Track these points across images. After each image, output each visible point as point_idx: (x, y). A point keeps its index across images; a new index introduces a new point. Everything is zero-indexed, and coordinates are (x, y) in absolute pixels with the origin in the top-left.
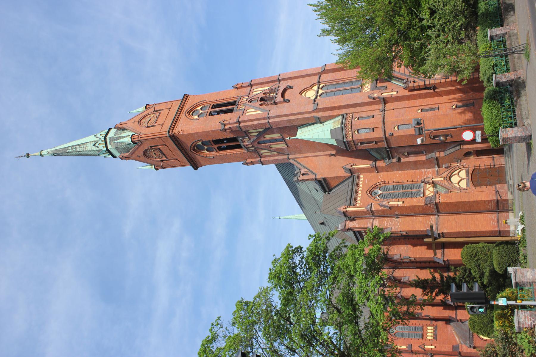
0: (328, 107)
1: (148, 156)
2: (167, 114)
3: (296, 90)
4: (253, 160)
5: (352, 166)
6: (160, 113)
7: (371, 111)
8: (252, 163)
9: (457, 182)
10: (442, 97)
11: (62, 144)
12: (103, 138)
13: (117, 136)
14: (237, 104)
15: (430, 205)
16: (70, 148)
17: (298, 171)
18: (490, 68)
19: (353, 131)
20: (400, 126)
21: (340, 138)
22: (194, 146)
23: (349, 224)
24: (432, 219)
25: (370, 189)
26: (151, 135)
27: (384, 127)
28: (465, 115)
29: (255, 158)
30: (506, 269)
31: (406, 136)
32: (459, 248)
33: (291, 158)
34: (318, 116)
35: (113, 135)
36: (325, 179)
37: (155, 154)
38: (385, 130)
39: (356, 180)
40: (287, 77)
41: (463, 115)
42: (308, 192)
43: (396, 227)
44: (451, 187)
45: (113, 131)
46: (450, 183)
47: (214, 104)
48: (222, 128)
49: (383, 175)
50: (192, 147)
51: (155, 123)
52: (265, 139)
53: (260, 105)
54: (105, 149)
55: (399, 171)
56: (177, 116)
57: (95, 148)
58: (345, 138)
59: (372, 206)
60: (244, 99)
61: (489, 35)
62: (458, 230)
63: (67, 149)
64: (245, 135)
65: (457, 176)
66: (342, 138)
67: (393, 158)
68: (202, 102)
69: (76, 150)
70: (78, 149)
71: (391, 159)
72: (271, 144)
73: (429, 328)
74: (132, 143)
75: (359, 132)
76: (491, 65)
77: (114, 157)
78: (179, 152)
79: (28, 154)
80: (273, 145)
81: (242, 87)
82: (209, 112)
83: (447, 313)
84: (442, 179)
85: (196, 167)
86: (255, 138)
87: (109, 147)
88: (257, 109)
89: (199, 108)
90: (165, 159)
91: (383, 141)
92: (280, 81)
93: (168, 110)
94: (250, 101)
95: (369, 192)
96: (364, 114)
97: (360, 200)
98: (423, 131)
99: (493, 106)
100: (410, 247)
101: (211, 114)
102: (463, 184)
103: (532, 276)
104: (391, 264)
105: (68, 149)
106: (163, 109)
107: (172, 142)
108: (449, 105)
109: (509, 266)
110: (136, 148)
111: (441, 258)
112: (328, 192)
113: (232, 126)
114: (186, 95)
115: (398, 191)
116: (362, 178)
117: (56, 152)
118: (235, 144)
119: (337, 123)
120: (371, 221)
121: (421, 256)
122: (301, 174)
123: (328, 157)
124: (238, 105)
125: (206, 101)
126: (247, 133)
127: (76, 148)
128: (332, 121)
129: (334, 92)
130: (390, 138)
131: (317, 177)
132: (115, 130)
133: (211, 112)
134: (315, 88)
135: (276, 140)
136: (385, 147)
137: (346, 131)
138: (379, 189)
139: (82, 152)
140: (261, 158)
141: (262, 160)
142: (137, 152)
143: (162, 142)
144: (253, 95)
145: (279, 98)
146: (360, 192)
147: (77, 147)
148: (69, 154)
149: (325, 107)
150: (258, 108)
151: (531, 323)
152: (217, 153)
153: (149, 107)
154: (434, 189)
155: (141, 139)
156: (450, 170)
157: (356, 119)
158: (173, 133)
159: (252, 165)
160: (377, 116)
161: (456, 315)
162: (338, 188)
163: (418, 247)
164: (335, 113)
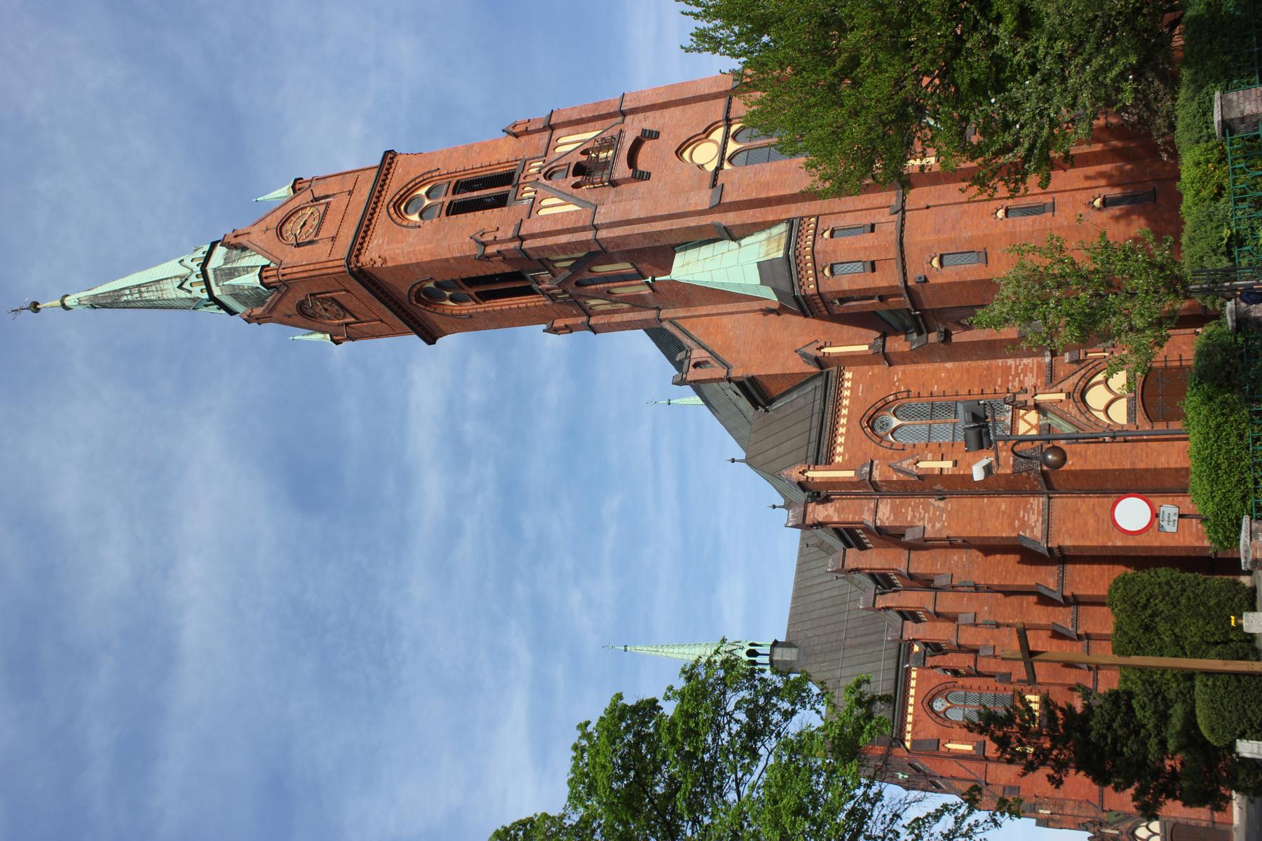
0: (751, 200)
1: (310, 314)
2: (344, 208)
3: (667, 143)
4: (569, 321)
5: (822, 348)
6: (328, 204)
7: (866, 209)
8: (569, 329)
9: (1102, 407)
10: (1065, 170)
11: (105, 282)
12: (199, 268)
13: (229, 266)
15: (1029, 474)
16: (127, 292)
17: (684, 357)
18: (1218, 247)
19: (819, 268)
20: (945, 257)
21: (785, 286)
22: (419, 290)
23: (813, 511)
24: (1032, 504)
25: (871, 412)
26: (307, 268)
27: (903, 259)
28: (1129, 224)
29: (575, 316)
30: (1234, 742)
31: (964, 283)
32: (1105, 564)
33: (665, 319)
34: (724, 223)
35: (222, 262)
36: (752, 379)
37: (326, 310)
38: (904, 267)
39: (834, 384)
40: (642, 104)
41: (1122, 223)
43: (938, 525)
44: (1085, 421)
45: (220, 251)
46: (1083, 409)
47: (458, 181)
48: (479, 253)
49: (904, 372)
50: (415, 290)
51: (317, 234)
52: (593, 276)
54: (205, 296)
55: (946, 362)
56: (368, 216)
57: (183, 294)
58: (796, 288)
59: (874, 467)
60: (536, 165)
61: (1217, 118)
62: (1101, 541)
63: (120, 294)
64: (542, 267)
65: (1102, 387)
66: (789, 285)
67: (929, 331)
68: (429, 175)
69: (141, 297)
70: (145, 295)
71: (925, 335)
72: (611, 285)
75: (835, 270)
76: (1222, 239)
77: (231, 312)
79: (36, 304)
80: (616, 287)
81: (527, 132)
82: (446, 204)
83: (1072, 677)
84: (1062, 396)
86: (568, 273)
87: (217, 292)
88: (568, 199)
89: (422, 191)
90: (353, 320)
91: (900, 295)
92: (624, 114)
93: (345, 197)
94: (549, 176)
95: (868, 422)
96: (848, 220)
98: (992, 438)
99: (1223, 414)
100: (977, 557)
102: (1119, 414)
105: (122, 295)
106: (334, 194)
107: (360, 286)
108: (1083, 197)
109: (1242, 736)
110: (277, 298)
111: (1055, 589)
112: (763, 407)
113: (503, 247)
114: (390, 155)
116: (848, 380)
117: (97, 301)
118: (518, 285)
120: (872, 505)
121: (1003, 583)
122: (692, 363)
123: (760, 316)
124: (518, 185)
125: (437, 173)
126: (545, 261)
127: (140, 292)
128: (763, 236)
129: (767, 149)
130: (919, 289)
131: (733, 374)
132: (224, 250)
133: (451, 202)
134: (718, 135)
135: (623, 277)
136: (908, 309)
138: (894, 413)
140: (589, 316)
141: (593, 321)
143: (337, 285)
144: (556, 156)
146: (843, 421)
147: (143, 289)
148: (128, 305)
149: (741, 199)
150: (567, 195)
152: (478, 306)
153: (300, 186)
154: (1039, 419)
155: (285, 278)
156: (1083, 372)
157: (827, 235)
158: (359, 265)
159: (567, 333)
160: (885, 227)
161: (1096, 681)
162: (787, 399)
163: (998, 556)
164: (769, 214)
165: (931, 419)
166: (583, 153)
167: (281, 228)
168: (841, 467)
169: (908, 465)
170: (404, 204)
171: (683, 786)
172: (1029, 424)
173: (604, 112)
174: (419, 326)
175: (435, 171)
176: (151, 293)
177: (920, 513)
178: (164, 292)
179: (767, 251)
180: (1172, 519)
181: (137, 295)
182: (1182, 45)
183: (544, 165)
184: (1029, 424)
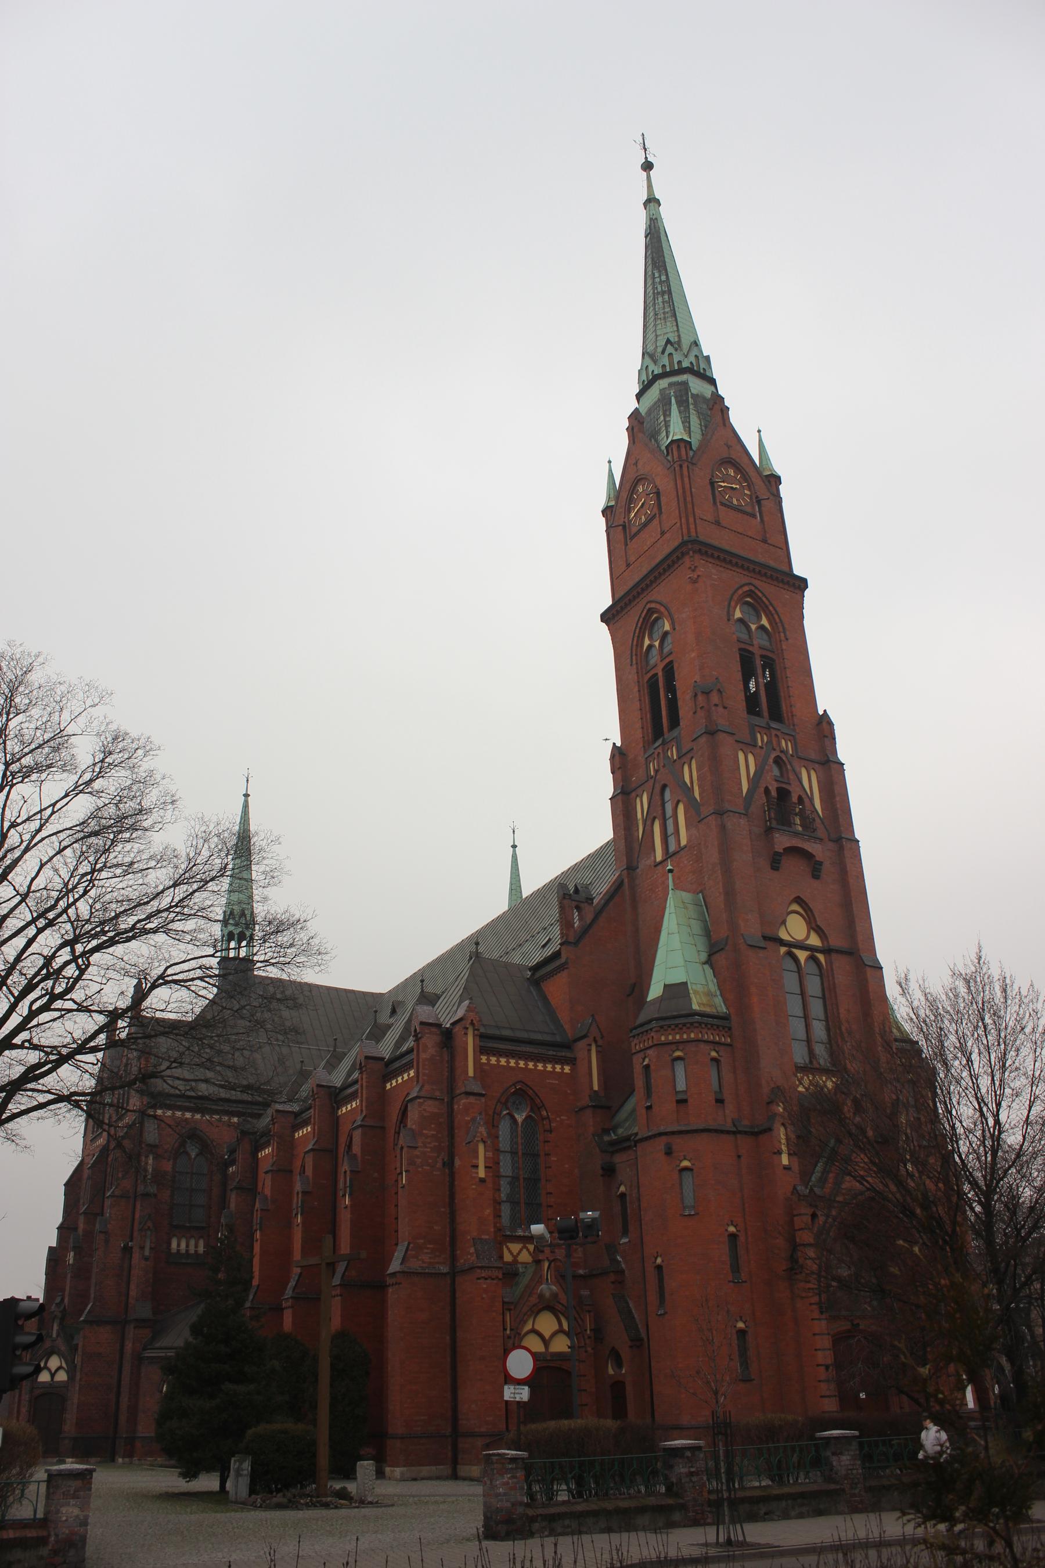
6: (754, 516)
9: (537, 1327)
13: (691, 400)
14: (774, 725)
16: (663, 278)
22: (657, 611)
25: (530, 1092)
26: (688, 493)
51: (722, 504)
65: (556, 1327)
69: (658, 293)
70: (660, 299)
73: (201, 1243)
78: (645, 570)
85: (609, 618)
87: (663, 383)
88: (754, 782)
89: (764, 622)
94: (778, 761)
97: (498, 1064)
103: (66, 1520)
104: (344, 1146)
105: (660, 272)
124: (769, 728)
125: (783, 638)
133: (753, 653)
134: (814, 940)
137: (673, 1027)
139: (652, 308)
145: (782, 841)
147: (666, 297)
157: (714, 1054)
165: (523, 1154)
166: (800, 798)
167: (730, 462)
168: (476, 1060)
169: (481, 1133)
170: (805, 915)
172: (518, 1254)
173: (841, 820)
174: (621, 607)
175: (785, 636)
177: (429, 1143)
179: (698, 992)
180: (516, 1396)
182: (75, 1255)
183: (789, 756)
184: (518, 1254)
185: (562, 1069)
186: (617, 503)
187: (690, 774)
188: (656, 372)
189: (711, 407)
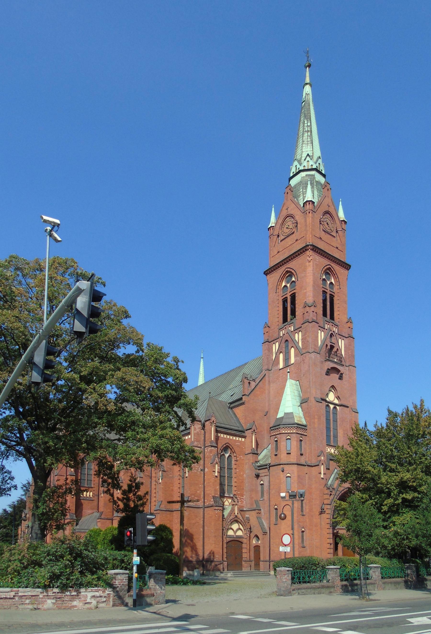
13: (315, 184)
16: (309, 124)
19: (290, 435)
21: (284, 422)
25: (231, 447)
35: (317, 180)
38: (288, 464)
42: (231, 386)
53: (327, 345)
69: (306, 131)
70: (306, 134)
74: (304, 202)
87: (303, 174)
88: (324, 342)
89: (333, 281)
101: (324, 292)
102: (230, 533)
105: (307, 121)
115: (226, 472)
119: (299, 420)
122: (250, 381)
127: (308, 131)
133: (327, 293)
134: (336, 401)
135: (287, 359)
142: (293, 205)
147: (309, 133)
151: (117, 585)
157: (301, 438)
171: (414, 466)
176: (306, 137)
178: (306, 145)
181: (306, 130)
185: (242, 439)
186: (276, 225)
187: (298, 337)
188: (300, 169)
189: (324, 188)
